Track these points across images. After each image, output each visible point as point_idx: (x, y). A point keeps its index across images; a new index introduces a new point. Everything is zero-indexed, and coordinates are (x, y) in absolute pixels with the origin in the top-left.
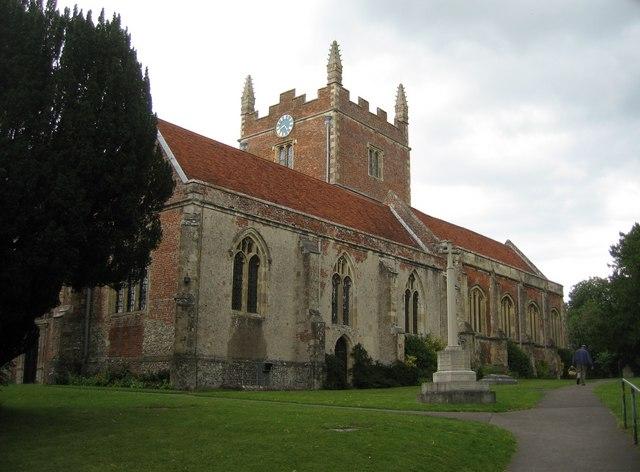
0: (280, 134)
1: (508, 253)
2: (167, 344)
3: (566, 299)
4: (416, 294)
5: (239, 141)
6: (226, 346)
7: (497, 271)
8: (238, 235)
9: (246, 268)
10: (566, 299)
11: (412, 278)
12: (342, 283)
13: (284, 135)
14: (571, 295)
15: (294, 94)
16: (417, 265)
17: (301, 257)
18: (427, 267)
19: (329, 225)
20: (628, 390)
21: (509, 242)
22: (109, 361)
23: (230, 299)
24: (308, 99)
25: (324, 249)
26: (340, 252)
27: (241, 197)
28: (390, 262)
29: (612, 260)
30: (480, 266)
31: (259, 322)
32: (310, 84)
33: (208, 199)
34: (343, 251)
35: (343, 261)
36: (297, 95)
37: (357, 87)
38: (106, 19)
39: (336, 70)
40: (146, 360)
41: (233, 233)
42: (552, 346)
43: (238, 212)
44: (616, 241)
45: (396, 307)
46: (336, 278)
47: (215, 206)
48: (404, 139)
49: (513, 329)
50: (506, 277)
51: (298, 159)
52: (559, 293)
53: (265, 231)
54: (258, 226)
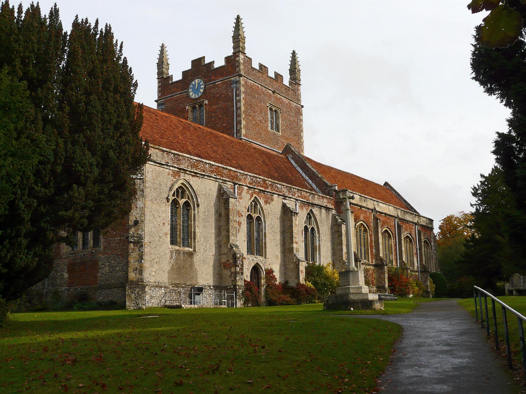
1: (387, 193)
2: (120, 274)
3: (436, 231)
4: (313, 229)
5: (156, 101)
7: (377, 209)
8: (173, 185)
9: (181, 211)
10: (436, 231)
11: (310, 216)
12: (255, 223)
13: (197, 96)
14: (440, 228)
15: (204, 61)
16: (313, 205)
17: (222, 201)
18: (321, 207)
19: (243, 175)
20: (489, 301)
21: (386, 184)
22: (69, 290)
23: (169, 236)
24: (216, 66)
25: (240, 194)
26: (252, 196)
27: (174, 154)
28: (290, 204)
29: (474, 200)
30: (364, 204)
31: (191, 255)
32: (218, 56)
34: (254, 195)
36: (207, 61)
37: (256, 52)
38: (99, 29)
39: (238, 39)
40: (101, 287)
42: (424, 270)
43: (173, 167)
44: (477, 181)
45: (297, 240)
46: (249, 217)
47: (155, 162)
48: (297, 98)
49: (393, 257)
50: (386, 214)
51: (280, 148)
52: (430, 226)
53: (195, 182)
54: (187, 177)
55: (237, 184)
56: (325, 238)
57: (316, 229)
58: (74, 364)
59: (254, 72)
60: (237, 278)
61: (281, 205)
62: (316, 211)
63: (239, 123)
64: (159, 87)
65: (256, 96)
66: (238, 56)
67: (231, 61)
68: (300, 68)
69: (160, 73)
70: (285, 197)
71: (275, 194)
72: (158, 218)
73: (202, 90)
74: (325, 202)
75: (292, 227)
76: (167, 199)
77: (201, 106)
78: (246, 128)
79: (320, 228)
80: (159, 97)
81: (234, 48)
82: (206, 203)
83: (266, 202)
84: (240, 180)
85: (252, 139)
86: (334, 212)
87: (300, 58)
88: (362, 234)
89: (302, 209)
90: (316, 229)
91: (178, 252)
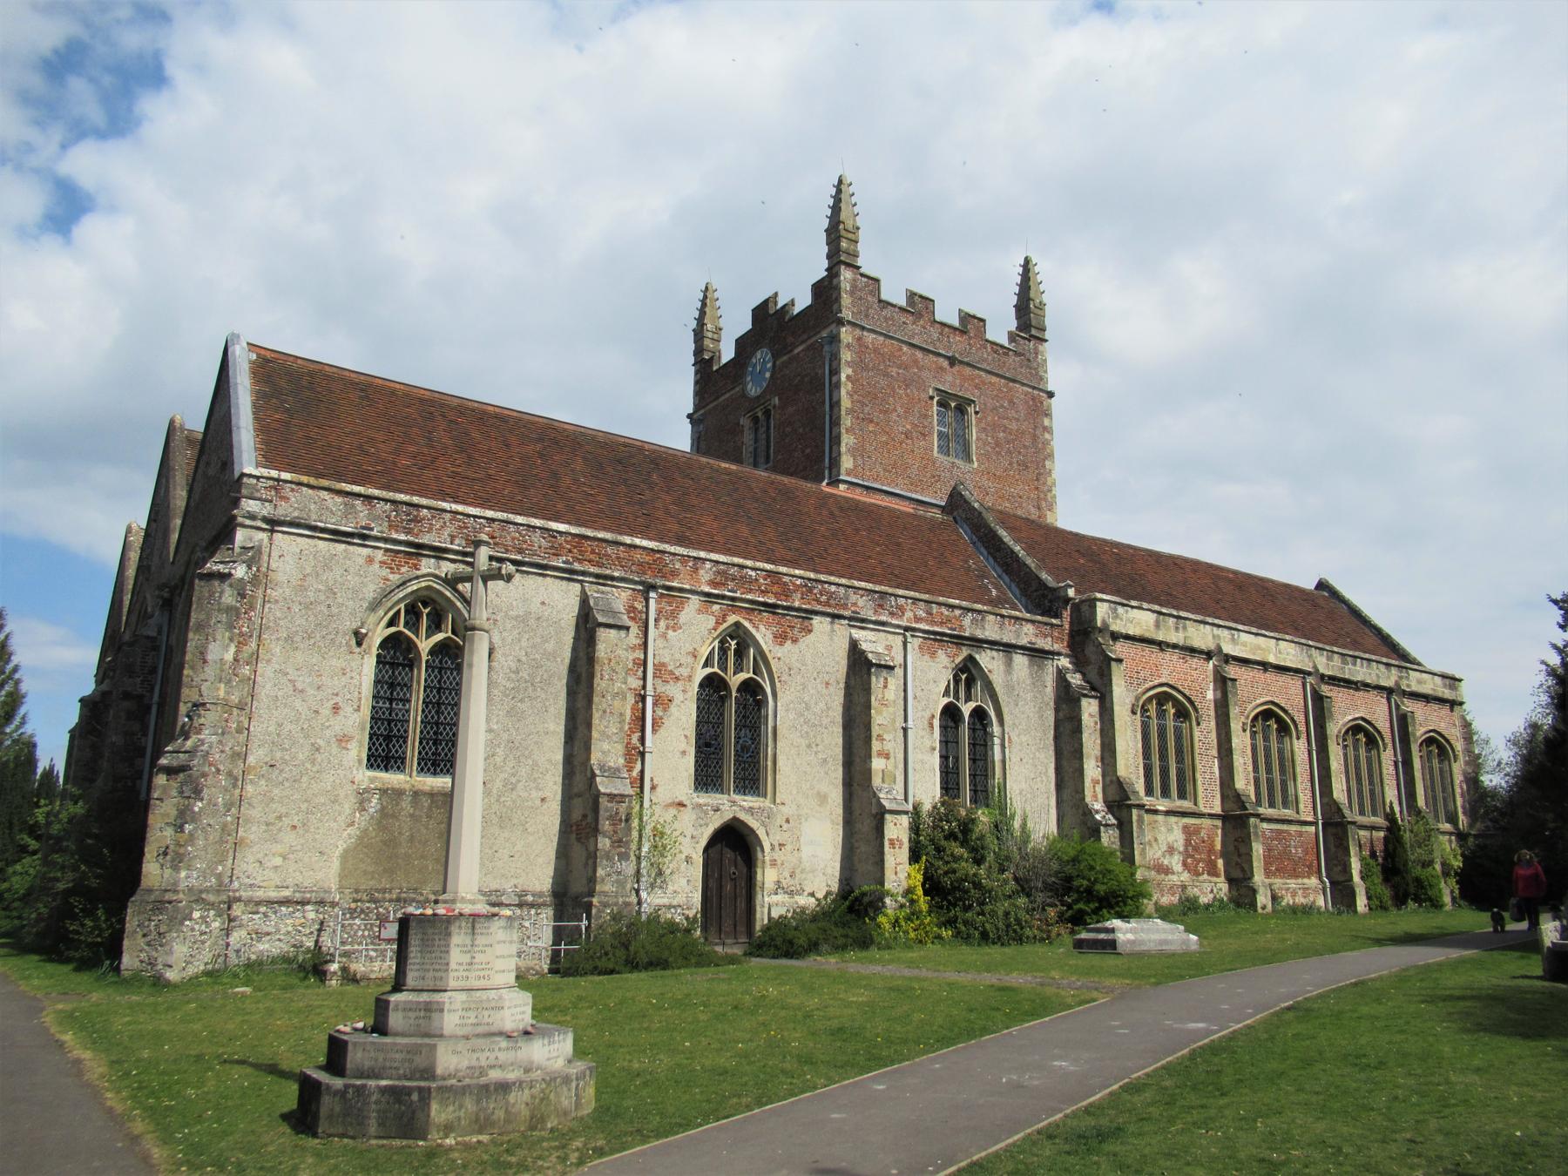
0: (753, 390)
6: (336, 864)
7: (1228, 649)
11: (968, 675)
16: (978, 643)
18: (1008, 648)
21: (1322, 585)
24: (797, 310)
28: (874, 643)
33: (284, 510)
35: (737, 644)
37: (892, 265)
39: (839, 236)
41: (370, 591)
55: (653, 587)
56: (1024, 739)
57: (992, 714)
58: (1399, 876)
59: (887, 312)
60: (600, 872)
61: (846, 646)
63: (836, 440)
64: (696, 383)
65: (894, 371)
66: (837, 275)
67: (825, 291)
68: (1045, 298)
69: (699, 351)
70: (858, 621)
71: (817, 613)
73: (768, 375)
74: (1027, 634)
75: (869, 707)
76: (359, 639)
77: (767, 413)
78: (855, 452)
79: (1005, 710)
80: (697, 407)
81: (829, 257)
82: (524, 643)
83: (781, 638)
84: (674, 574)
85: (875, 480)
86: (1064, 662)
88: (1170, 723)
89: (933, 655)
90: (992, 714)
91: (391, 795)
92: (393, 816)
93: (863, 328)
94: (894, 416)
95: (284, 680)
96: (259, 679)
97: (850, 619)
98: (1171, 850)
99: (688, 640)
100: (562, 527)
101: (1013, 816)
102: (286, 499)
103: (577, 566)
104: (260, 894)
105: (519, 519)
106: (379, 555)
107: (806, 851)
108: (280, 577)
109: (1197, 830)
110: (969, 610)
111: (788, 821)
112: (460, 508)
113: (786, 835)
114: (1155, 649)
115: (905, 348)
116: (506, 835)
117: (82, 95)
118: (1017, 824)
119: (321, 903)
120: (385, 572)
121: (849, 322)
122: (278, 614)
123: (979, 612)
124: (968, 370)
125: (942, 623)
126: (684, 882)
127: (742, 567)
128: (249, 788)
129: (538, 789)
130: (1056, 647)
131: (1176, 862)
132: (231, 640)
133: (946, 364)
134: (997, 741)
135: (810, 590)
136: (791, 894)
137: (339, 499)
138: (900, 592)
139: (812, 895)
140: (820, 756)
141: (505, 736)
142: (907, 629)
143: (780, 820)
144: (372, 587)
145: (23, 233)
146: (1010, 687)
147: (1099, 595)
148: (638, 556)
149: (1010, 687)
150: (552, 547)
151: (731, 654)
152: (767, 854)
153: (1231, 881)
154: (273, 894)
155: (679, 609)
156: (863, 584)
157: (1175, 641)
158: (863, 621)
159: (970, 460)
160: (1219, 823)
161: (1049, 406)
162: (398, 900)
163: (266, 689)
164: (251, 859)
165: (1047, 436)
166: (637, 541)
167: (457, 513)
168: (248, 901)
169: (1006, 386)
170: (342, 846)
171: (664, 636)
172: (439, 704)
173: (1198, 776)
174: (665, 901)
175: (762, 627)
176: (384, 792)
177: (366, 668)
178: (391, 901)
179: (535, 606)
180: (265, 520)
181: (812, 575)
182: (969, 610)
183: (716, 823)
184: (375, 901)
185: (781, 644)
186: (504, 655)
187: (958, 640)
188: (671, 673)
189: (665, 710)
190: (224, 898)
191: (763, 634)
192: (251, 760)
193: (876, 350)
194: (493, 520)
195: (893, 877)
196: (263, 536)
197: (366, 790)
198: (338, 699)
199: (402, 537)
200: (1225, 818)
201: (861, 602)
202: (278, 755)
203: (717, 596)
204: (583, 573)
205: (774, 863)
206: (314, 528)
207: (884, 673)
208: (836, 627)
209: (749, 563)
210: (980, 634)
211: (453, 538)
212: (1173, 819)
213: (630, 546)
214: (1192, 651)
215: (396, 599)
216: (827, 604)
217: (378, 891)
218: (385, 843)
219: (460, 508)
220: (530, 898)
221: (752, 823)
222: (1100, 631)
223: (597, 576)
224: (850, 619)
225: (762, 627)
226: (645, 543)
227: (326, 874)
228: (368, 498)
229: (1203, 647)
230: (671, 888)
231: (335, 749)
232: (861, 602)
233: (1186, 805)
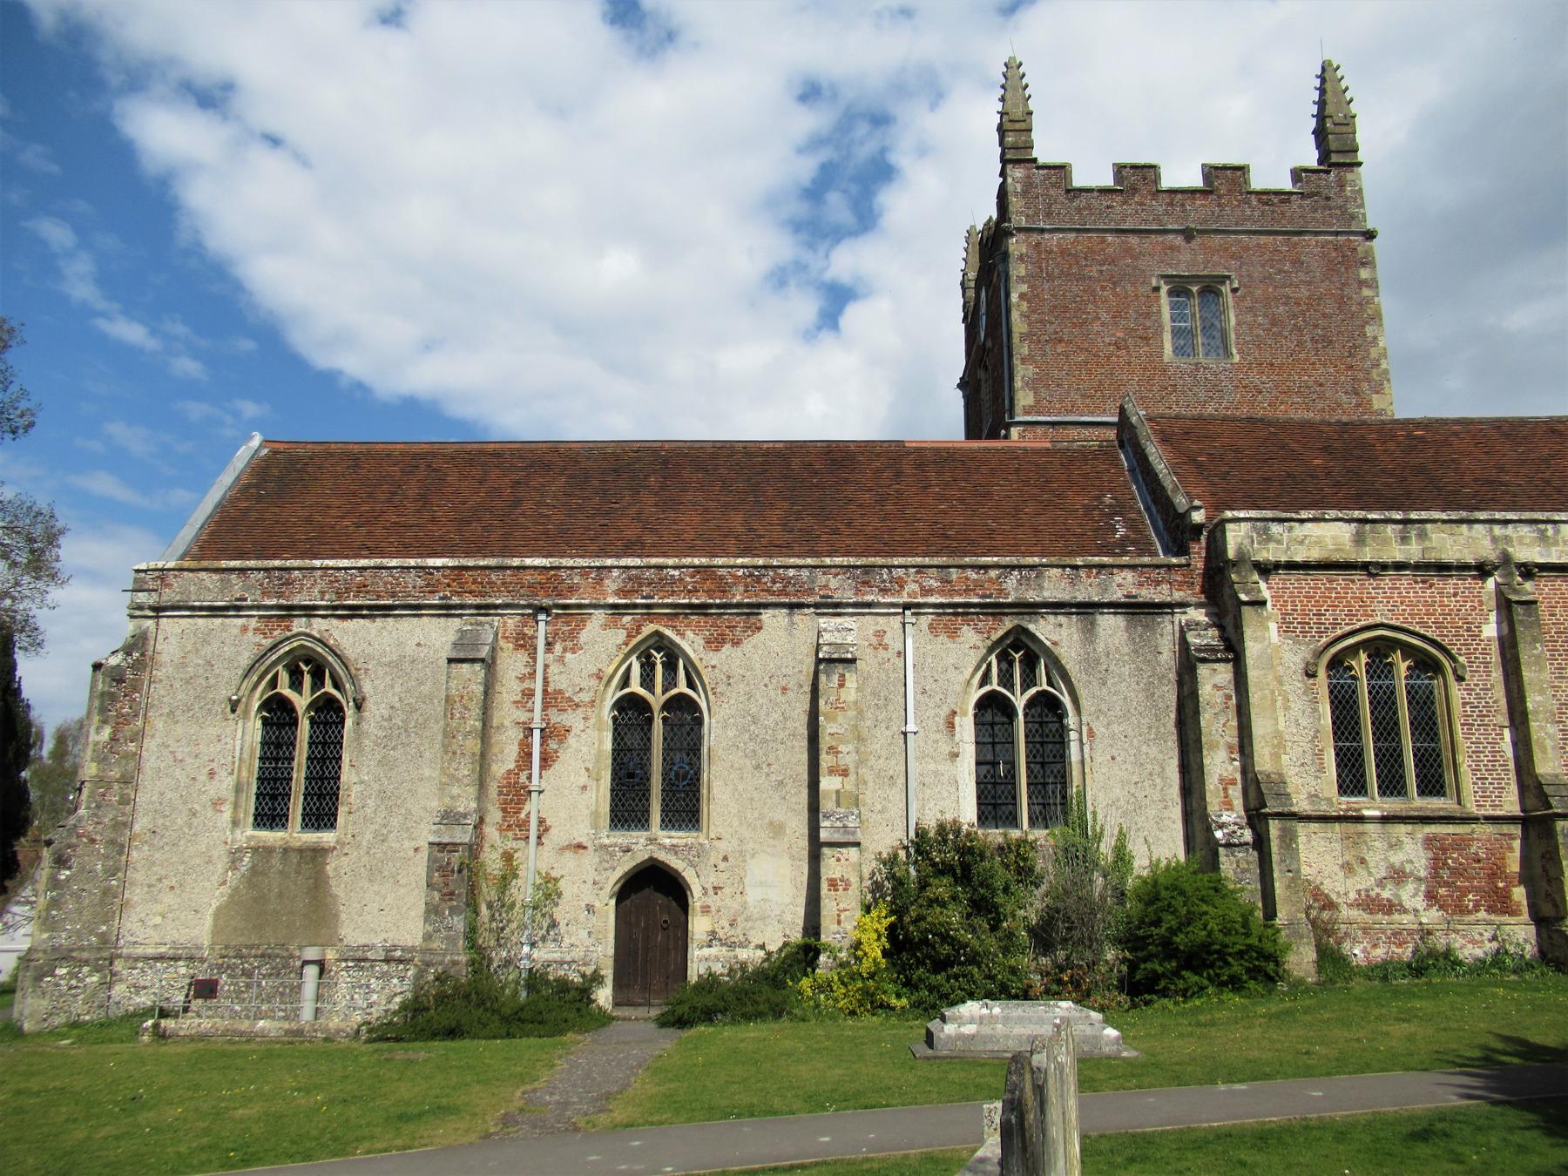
11: (1020, 652)
16: (1032, 609)
18: (1086, 609)
33: (169, 596)
41: (245, 660)
57: (1066, 700)
59: (1082, 201)
62: (1044, 629)
70: (831, 607)
71: (766, 606)
72: (189, 760)
82: (398, 689)
83: (715, 643)
85: (1069, 412)
87: (1353, 82)
89: (953, 634)
92: (263, 874)
93: (1042, 231)
94: (1096, 327)
95: (166, 752)
96: (144, 754)
97: (816, 606)
98: (1398, 876)
99: (597, 657)
100: (439, 562)
101: (1099, 838)
102: (169, 586)
103: (456, 600)
104: (140, 951)
105: (394, 562)
106: (253, 623)
107: (753, 895)
108: (164, 658)
109: (1461, 844)
110: (1013, 567)
111: (725, 859)
112: (330, 563)
113: (724, 876)
114: (1358, 576)
115: (1109, 238)
116: (376, 888)
117: (837, 206)
118: (1106, 848)
119: (191, 959)
120: (259, 638)
121: (1020, 230)
122: (162, 692)
123: (1032, 567)
124: (1217, 239)
125: (967, 591)
126: (584, 934)
127: (660, 568)
128: (135, 854)
129: (411, 839)
130: (1178, 596)
131: (1411, 896)
132: (105, 722)
133: (1179, 240)
134: (1073, 735)
135: (758, 580)
136: (732, 946)
137: (215, 577)
138: (896, 561)
139: (762, 947)
140: (773, 777)
141: (376, 787)
142: (906, 606)
143: (714, 858)
144: (246, 654)
145: (810, 335)
146: (1091, 663)
147: (1229, 514)
148: (528, 577)
149: (1091, 663)
150: (428, 585)
151: (659, 668)
152: (697, 897)
153: (1539, 920)
154: (150, 951)
155: (582, 624)
156: (838, 560)
157: (1399, 557)
158: (837, 605)
159: (1229, 355)
160: (1516, 830)
161: (1369, 252)
162: (262, 956)
163: (150, 760)
164: (135, 918)
165: (1366, 292)
166: (528, 562)
167: (327, 568)
168: (128, 957)
169: (1287, 243)
170: (215, 904)
171: (561, 660)
172: (323, 760)
173: (1460, 758)
174: (557, 956)
175: (689, 634)
176: (255, 850)
177: (251, 731)
178: (255, 956)
179: (410, 648)
180: (152, 608)
181: (761, 562)
182: (1013, 567)
183: (626, 865)
184: (239, 956)
185: (717, 650)
186: (376, 703)
187: (996, 610)
188: (570, 699)
189: (561, 742)
190: (106, 954)
191: (690, 642)
192: (137, 828)
193: (1064, 252)
194: (365, 568)
195: (834, 927)
196: (150, 623)
197: (239, 850)
198: (214, 765)
199: (274, 602)
200: (1525, 821)
201: (834, 583)
202: (160, 821)
203: (626, 606)
204: (462, 607)
205: (706, 910)
206: (193, 608)
207: (840, 668)
208: (797, 618)
209: (670, 562)
210: (1032, 596)
211: (322, 593)
212: (1401, 829)
213: (518, 568)
214: (1442, 568)
215: (268, 662)
216: (782, 592)
217: (246, 947)
218: (255, 900)
219: (330, 563)
220: (398, 953)
221: (675, 863)
222: (1234, 564)
223: (478, 607)
224: (816, 606)
225: (689, 634)
226: (537, 562)
227: (199, 931)
228: (242, 570)
229: (1470, 560)
230: (567, 941)
231: (210, 812)
232: (834, 583)
233: (1435, 804)
